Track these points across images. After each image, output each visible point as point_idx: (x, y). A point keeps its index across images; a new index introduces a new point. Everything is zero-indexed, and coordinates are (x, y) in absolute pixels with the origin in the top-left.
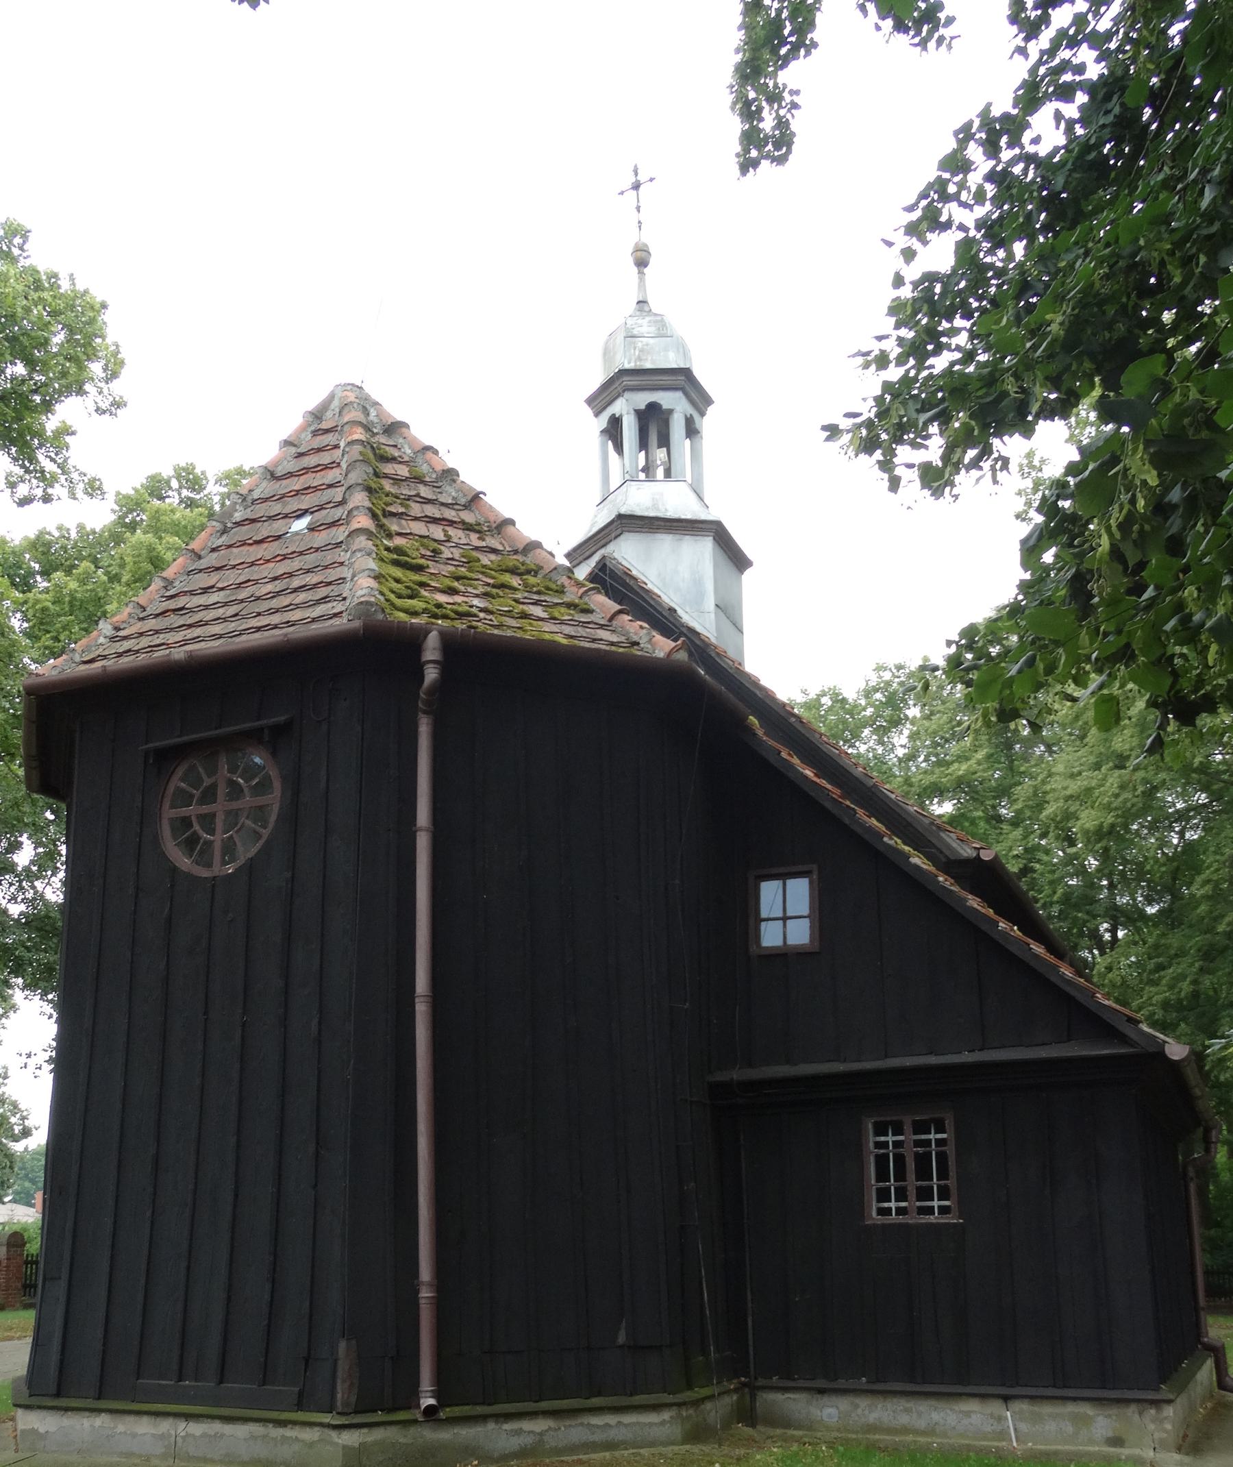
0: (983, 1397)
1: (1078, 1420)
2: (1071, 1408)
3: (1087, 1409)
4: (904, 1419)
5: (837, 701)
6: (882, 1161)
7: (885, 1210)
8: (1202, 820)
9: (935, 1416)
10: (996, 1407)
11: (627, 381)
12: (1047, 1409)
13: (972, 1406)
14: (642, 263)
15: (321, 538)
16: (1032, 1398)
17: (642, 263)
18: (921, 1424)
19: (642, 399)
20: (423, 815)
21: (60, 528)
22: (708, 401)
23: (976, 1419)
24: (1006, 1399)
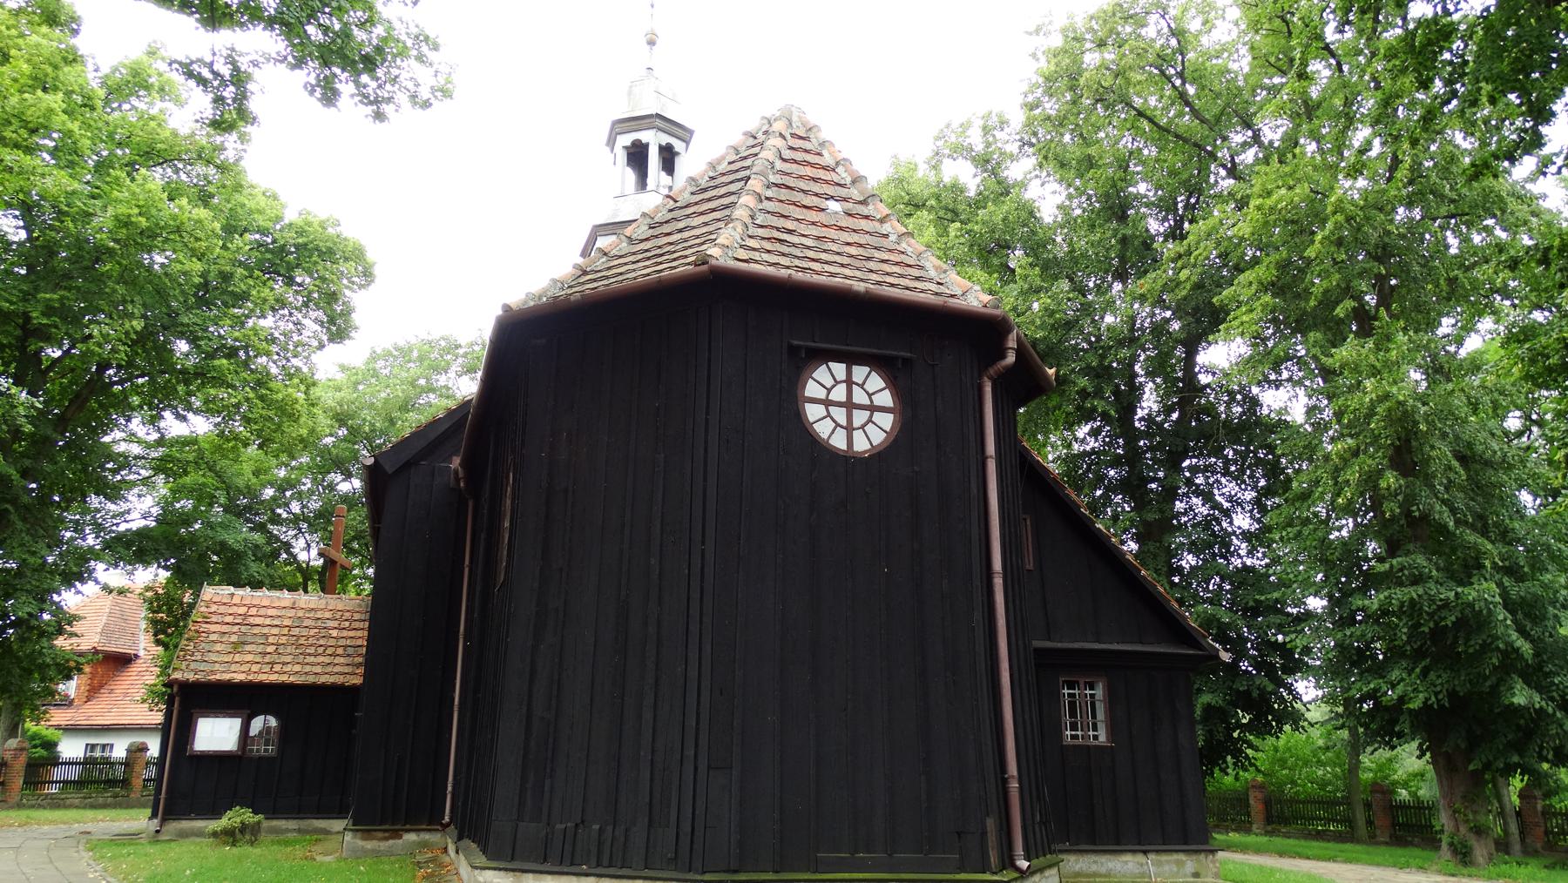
0: (1134, 852)
1: (1180, 864)
2: (1175, 857)
3: (1182, 857)
4: (1094, 868)
5: (135, 342)
6: (1072, 705)
7: (1102, 738)
8: (104, 470)
9: (1110, 865)
10: (1140, 858)
11: (658, 122)
12: (1164, 858)
13: (1128, 857)
14: (651, 43)
15: (846, 222)
16: (1157, 851)
17: (651, 43)
18: (1103, 870)
19: (665, 139)
20: (991, 448)
21: (329, 95)
22: (691, 132)
23: (1130, 865)
24: (1145, 852)
